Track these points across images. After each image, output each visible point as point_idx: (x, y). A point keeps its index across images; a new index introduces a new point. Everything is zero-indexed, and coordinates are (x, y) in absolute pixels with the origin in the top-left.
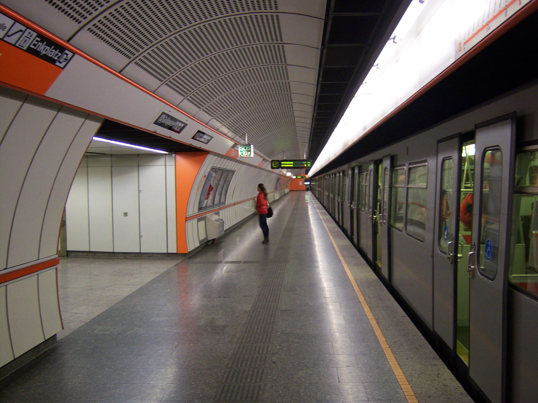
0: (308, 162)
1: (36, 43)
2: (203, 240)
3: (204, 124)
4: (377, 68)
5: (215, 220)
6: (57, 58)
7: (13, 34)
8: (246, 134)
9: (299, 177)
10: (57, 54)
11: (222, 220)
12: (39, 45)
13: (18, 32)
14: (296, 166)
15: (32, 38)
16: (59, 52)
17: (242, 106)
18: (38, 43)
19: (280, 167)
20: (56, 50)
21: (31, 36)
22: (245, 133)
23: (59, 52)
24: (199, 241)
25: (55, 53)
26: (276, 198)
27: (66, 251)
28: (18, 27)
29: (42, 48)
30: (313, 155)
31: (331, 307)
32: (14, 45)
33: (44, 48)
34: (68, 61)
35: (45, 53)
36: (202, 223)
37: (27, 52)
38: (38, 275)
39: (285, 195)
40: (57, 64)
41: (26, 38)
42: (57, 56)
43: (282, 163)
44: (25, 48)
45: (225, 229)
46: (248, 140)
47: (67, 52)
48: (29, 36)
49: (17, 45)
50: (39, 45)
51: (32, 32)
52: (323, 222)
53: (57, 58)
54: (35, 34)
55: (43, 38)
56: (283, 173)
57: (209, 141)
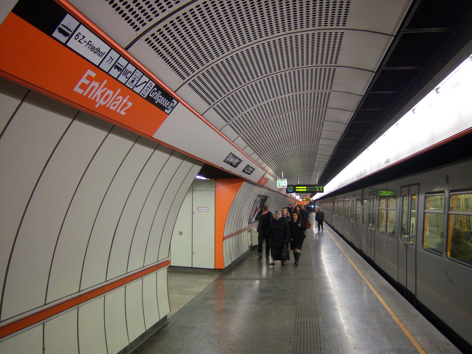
0: (320, 187)
1: (87, 82)
3: (254, 161)
4: (413, 112)
7: (140, 85)
8: (282, 171)
10: (126, 105)
12: (94, 87)
13: (143, 83)
14: (308, 190)
18: (90, 84)
19: (294, 191)
20: (124, 98)
21: (151, 86)
22: (282, 171)
23: (129, 100)
25: (122, 102)
28: (145, 79)
29: (99, 93)
32: (139, 94)
33: (103, 94)
34: (173, 108)
35: (103, 103)
36: (250, 233)
40: (166, 111)
41: (148, 88)
43: (296, 188)
44: (145, 97)
46: (283, 175)
47: (174, 101)
48: (150, 87)
49: (141, 94)
50: (94, 87)
51: (153, 83)
54: (154, 85)
55: (159, 87)
56: (293, 197)
57: (252, 172)
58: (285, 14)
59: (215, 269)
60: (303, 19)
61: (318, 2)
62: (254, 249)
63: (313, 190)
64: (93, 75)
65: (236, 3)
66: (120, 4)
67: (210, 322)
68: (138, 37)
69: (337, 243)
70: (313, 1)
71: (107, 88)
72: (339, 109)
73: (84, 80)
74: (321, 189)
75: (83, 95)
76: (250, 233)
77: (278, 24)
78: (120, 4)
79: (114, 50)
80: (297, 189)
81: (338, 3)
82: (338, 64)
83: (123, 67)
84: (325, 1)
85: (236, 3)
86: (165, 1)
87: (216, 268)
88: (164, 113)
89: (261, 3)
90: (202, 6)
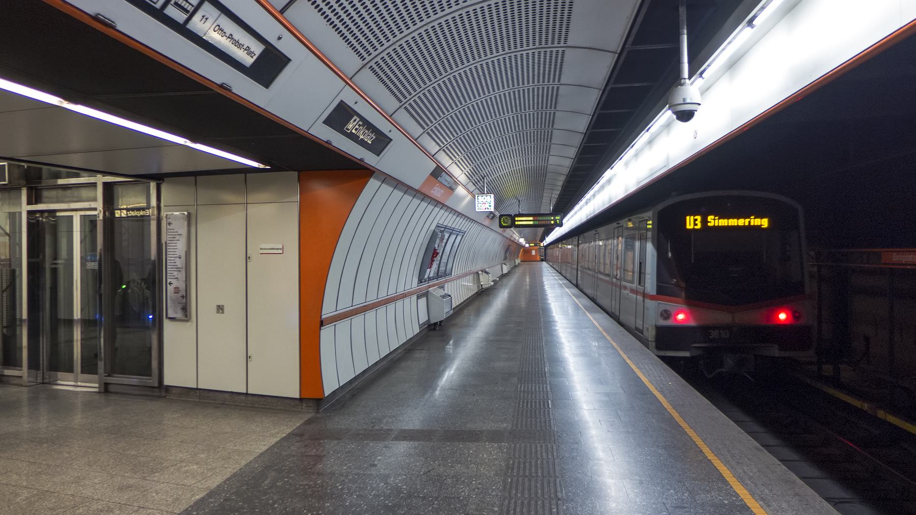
0: (557, 218)
2: (424, 324)
5: (441, 296)
9: (533, 245)
11: (450, 296)
14: (537, 223)
16: (374, 135)
17: (509, 166)
19: (513, 225)
20: (372, 134)
23: (374, 135)
24: (419, 325)
26: (505, 271)
30: (565, 205)
31: (585, 406)
36: (423, 301)
38: (335, 325)
39: (515, 266)
43: (516, 219)
45: (454, 306)
52: (573, 297)
58: (502, 15)
59: (301, 399)
60: (485, 18)
61: (545, 2)
62: (434, 329)
63: (543, 222)
65: (421, 3)
66: (322, 5)
69: (589, 315)
70: (540, 1)
72: (571, 110)
74: (558, 221)
76: (423, 301)
77: (449, 23)
78: (322, 5)
80: (518, 221)
81: (567, 4)
82: (569, 43)
84: (552, 2)
85: (421, 3)
86: (359, 2)
87: (303, 397)
89: (406, 4)
90: (493, 6)
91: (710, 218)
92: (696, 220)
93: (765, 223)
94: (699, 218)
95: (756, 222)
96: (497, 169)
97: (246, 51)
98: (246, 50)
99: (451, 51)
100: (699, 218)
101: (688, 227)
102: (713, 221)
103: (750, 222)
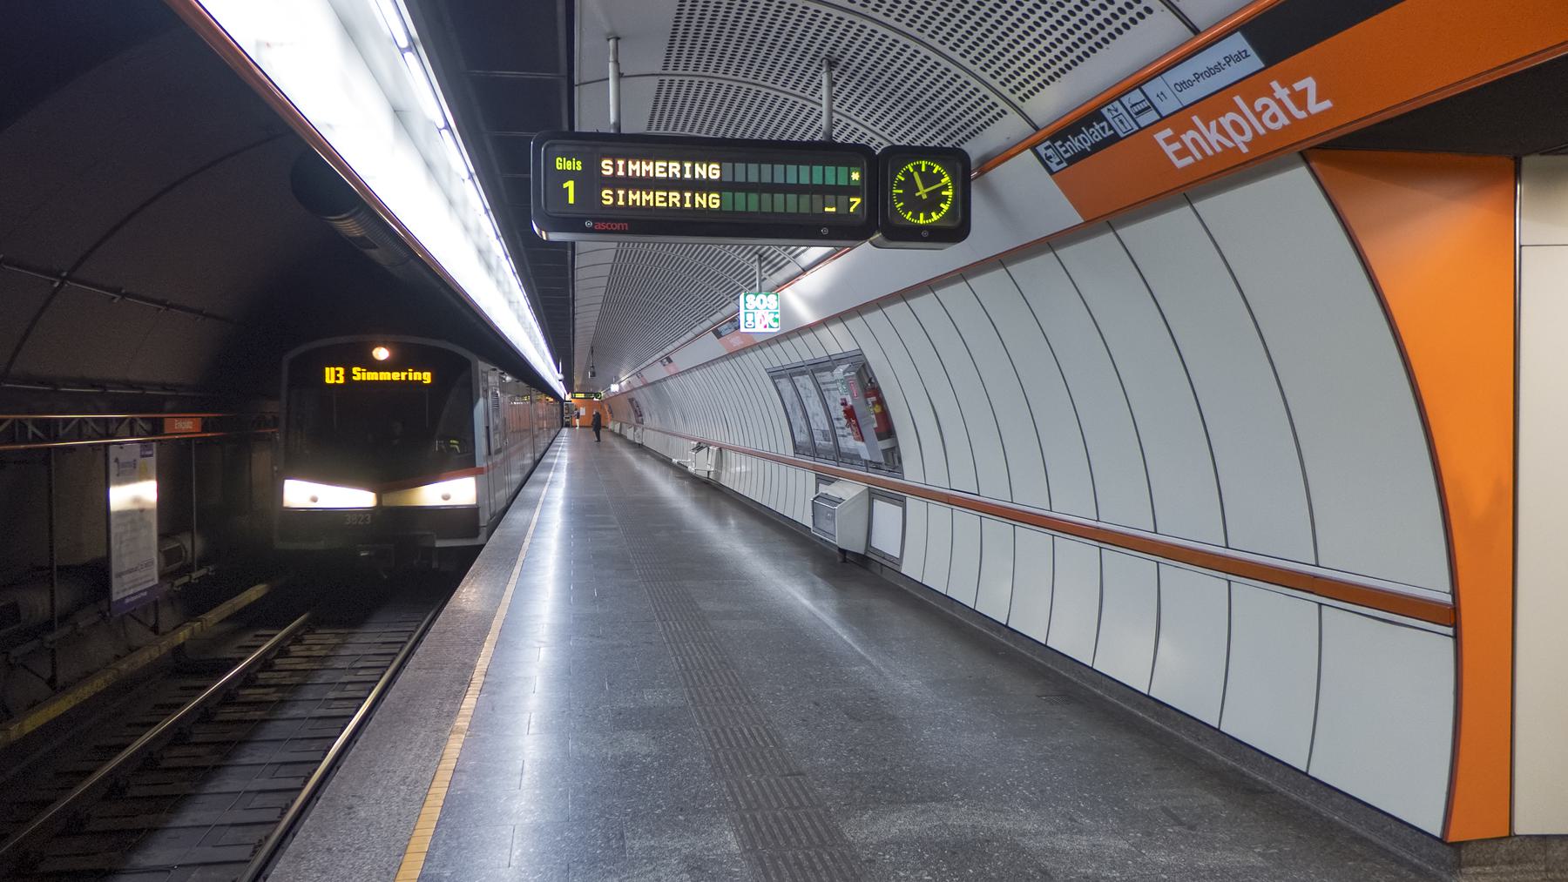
6: (1109, 130)
15: (1121, 109)
20: (1093, 126)
21: (1116, 110)
27: (867, 441)
29: (1077, 144)
31: (87, 689)
37: (1270, 66)
42: (1107, 129)
48: (1115, 114)
53: (1109, 130)
64: (1168, 132)
67: (915, 737)
68: (1168, 7)
71: (1212, 120)
73: (1170, 150)
75: (1334, 104)
79: (1123, 96)
82: (656, 80)
83: (1144, 100)
88: (1125, 140)
91: (355, 370)
92: (337, 372)
93: (427, 377)
94: (341, 370)
95: (417, 376)
96: (634, 256)
97: (1232, 63)
98: (1197, 79)
99: (719, 260)
100: (341, 370)
101: (328, 381)
102: (359, 374)
103: (407, 376)
